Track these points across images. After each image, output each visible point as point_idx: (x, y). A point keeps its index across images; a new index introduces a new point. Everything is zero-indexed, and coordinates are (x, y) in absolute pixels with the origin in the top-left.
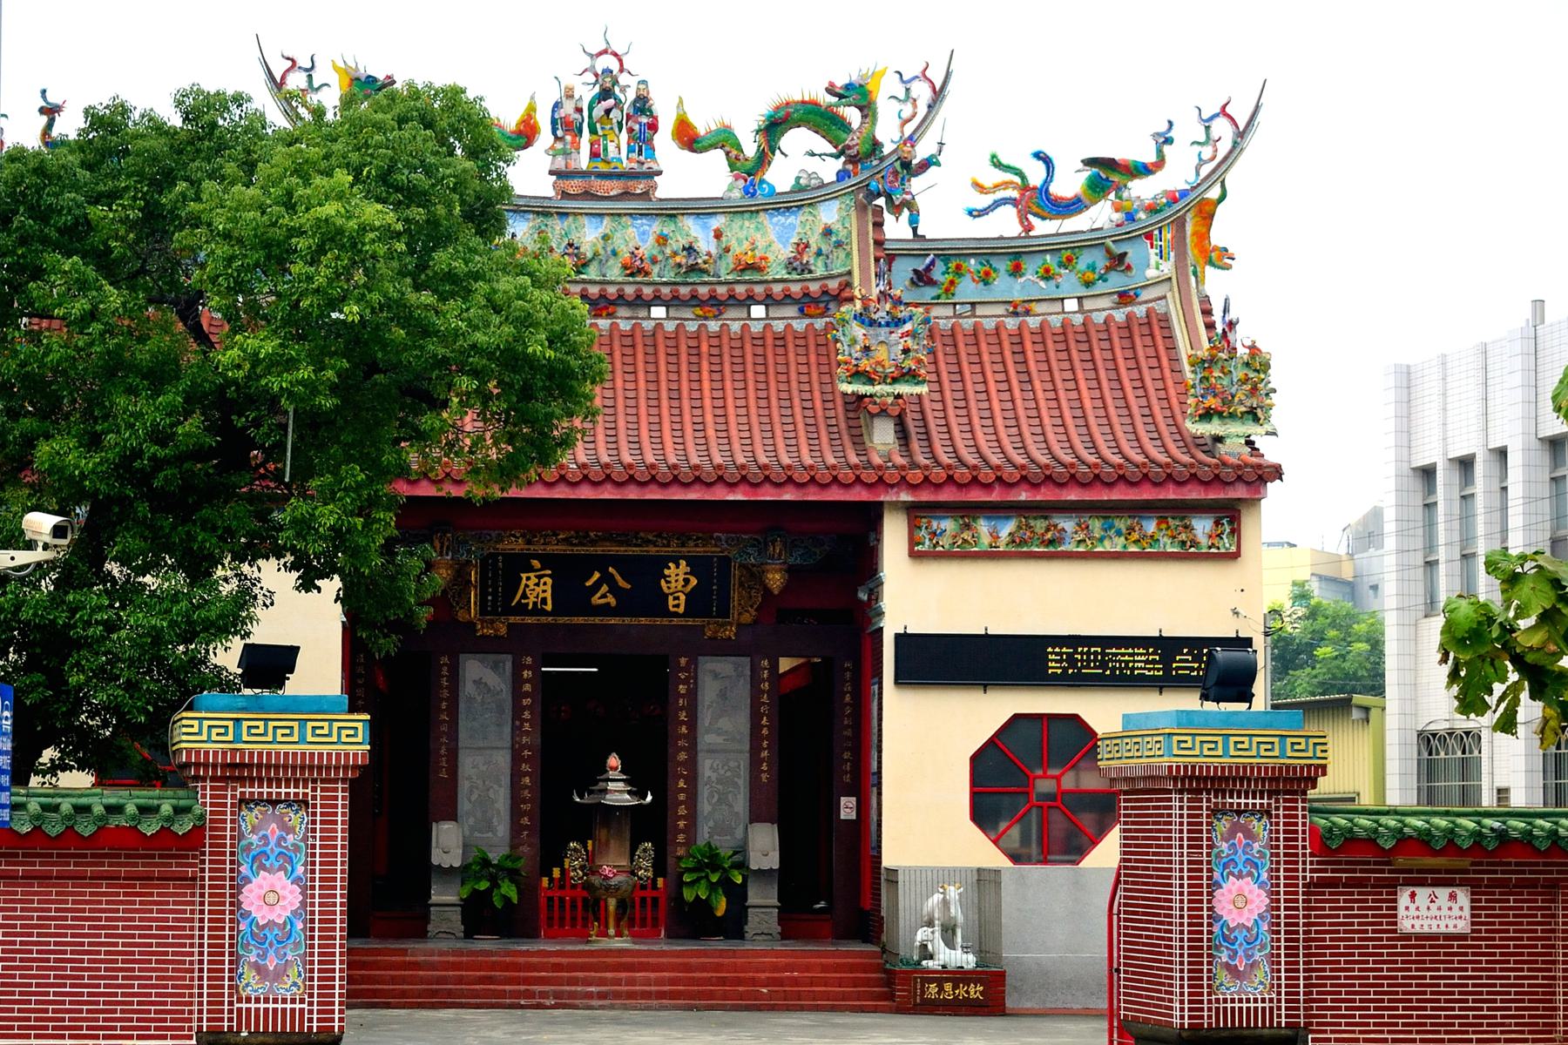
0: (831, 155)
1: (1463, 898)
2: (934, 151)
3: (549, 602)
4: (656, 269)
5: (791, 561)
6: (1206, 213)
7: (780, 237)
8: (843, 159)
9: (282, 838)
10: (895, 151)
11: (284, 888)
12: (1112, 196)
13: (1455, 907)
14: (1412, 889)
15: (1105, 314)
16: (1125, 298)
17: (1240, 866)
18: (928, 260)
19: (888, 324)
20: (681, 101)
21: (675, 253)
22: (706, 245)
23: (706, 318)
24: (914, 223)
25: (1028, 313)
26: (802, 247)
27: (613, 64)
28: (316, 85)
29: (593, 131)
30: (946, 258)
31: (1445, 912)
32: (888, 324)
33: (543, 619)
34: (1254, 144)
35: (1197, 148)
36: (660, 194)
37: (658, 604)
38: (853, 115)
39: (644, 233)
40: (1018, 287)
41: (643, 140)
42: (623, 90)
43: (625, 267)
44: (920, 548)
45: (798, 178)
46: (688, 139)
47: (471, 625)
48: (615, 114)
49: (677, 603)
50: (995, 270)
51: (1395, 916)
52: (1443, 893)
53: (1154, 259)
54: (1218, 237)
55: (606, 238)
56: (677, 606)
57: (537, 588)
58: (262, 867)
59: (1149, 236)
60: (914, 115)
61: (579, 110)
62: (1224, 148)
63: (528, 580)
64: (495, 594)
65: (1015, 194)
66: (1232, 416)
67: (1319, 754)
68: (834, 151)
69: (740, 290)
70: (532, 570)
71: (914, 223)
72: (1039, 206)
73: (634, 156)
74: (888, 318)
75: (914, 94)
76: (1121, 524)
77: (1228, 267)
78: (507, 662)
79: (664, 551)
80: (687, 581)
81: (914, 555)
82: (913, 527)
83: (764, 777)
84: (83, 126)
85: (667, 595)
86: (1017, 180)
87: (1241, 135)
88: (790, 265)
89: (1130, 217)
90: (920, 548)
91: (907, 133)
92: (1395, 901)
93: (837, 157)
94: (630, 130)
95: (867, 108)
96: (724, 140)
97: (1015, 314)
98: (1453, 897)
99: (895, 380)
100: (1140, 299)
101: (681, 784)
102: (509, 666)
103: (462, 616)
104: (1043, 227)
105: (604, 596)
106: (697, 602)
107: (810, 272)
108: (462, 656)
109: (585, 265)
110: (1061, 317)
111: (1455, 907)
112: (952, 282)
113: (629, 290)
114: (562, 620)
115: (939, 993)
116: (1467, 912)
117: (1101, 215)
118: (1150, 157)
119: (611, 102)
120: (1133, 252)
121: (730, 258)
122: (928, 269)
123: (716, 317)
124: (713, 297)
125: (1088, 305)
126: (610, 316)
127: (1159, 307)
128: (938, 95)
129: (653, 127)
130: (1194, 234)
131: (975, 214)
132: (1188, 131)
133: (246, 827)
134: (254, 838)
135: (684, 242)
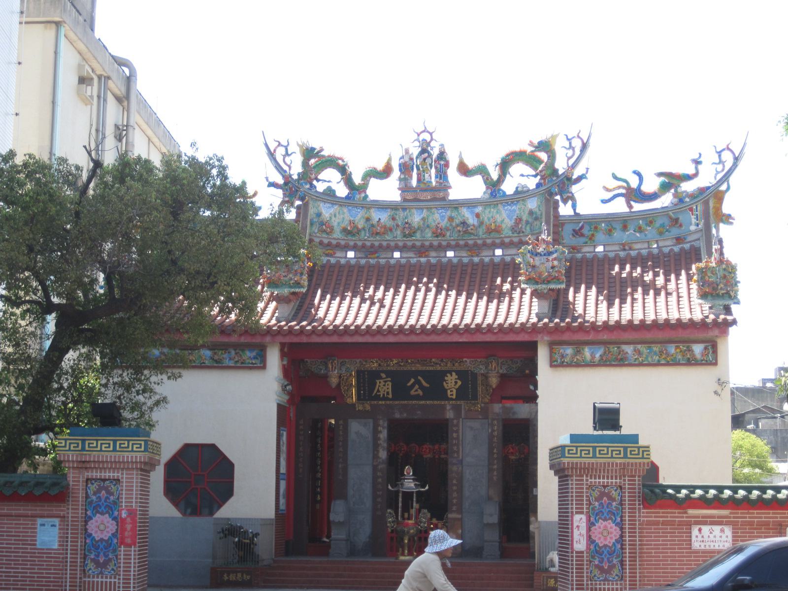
0: (533, 176)
1: (728, 531)
2: (584, 172)
3: (390, 393)
4: (448, 234)
5: (501, 371)
6: (719, 197)
7: (508, 216)
8: (539, 177)
9: (107, 498)
10: (564, 173)
11: (108, 522)
12: (673, 191)
13: (724, 536)
14: (699, 526)
15: (669, 248)
16: (679, 240)
17: (605, 514)
18: (580, 225)
19: (545, 255)
20: (461, 153)
21: (457, 226)
22: (472, 221)
23: (472, 256)
24: (574, 207)
25: (631, 249)
26: (519, 220)
27: (428, 138)
28: (289, 153)
29: (418, 169)
30: (590, 224)
31: (718, 538)
32: (545, 255)
33: (388, 402)
34: (742, 164)
35: (715, 166)
36: (451, 198)
37: (441, 394)
38: (543, 156)
39: (443, 216)
40: (625, 237)
41: (442, 174)
42: (432, 149)
43: (433, 233)
44: (555, 363)
45: (517, 188)
46: (464, 170)
47: (353, 405)
48: (428, 161)
49: (452, 393)
50: (615, 229)
51: (691, 540)
52: (717, 529)
53: (694, 221)
54: (726, 209)
55: (423, 219)
56: (452, 395)
57: (384, 387)
58: (98, 512)
59: (691, 210)
60: (573, 155)
61: (411, 159)
62: (728, 165)
63: (380, 384)
64: (364, 390)
65: (624, 191)
66: (718, 295)
67: (645, 456)
68: (534, 173)
69: (489, 241)
70: (381, 378)
71: (574, 207)
72: (635, 197)
73: (438, 180)
74: (545, 251)
75: (573, 145)
76: (656, 348)
77: (731, 223)
78: (371, 421)
79: (444, 369)
80: (456, 383)
81: (552, 366)
82: (551, 352)
83: (495, 478)
84: (724, 231)
85: (447, 390)
86: (625, 184)
87: (736, 159)
88: (513, 229)
89: (681, 201)
90: (555, 363)
91: (570, 164)
92: (691, 533)
93: (535, 176)
94: (436, 168)
95: (552, 155)
96: (482, 170)
97: (624, 250)
98: (722, 531)
99: (549, 282)
100: (687, 241)
101: (455, 482)
102: (371, 425)
103: (349, 401)
104: (638, 207)
105: (416, 391)
106: (462, 393)
107: (523, 232)
108: (350, 420)
109: (414, 232)
110: (647, 250)
111: (724, 536)
112: (593, 235)
113: (435, 243)
114: (397, 402)
115: (555, 584)
116: (730, 539)
117: (666, 200)
118: (691, 170)
119: (426, 155)
120: (682, 218)
121: (484, 227)
122: (582, 228)
123: (477, 256)
124: (475, 244)
125: (661, 244)
126: (426, 256)
127: (696, 244)
128: (584, 146)
129: (447, 165)
130: (714, 207)
131: (604, 202)
132: (709, 158)
133: (90, 492)
134: (94, 498)
135: (461, 220)
